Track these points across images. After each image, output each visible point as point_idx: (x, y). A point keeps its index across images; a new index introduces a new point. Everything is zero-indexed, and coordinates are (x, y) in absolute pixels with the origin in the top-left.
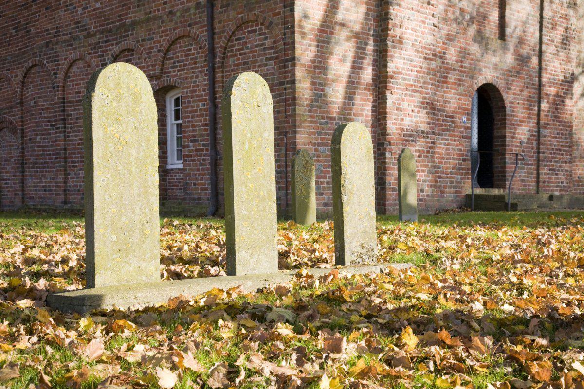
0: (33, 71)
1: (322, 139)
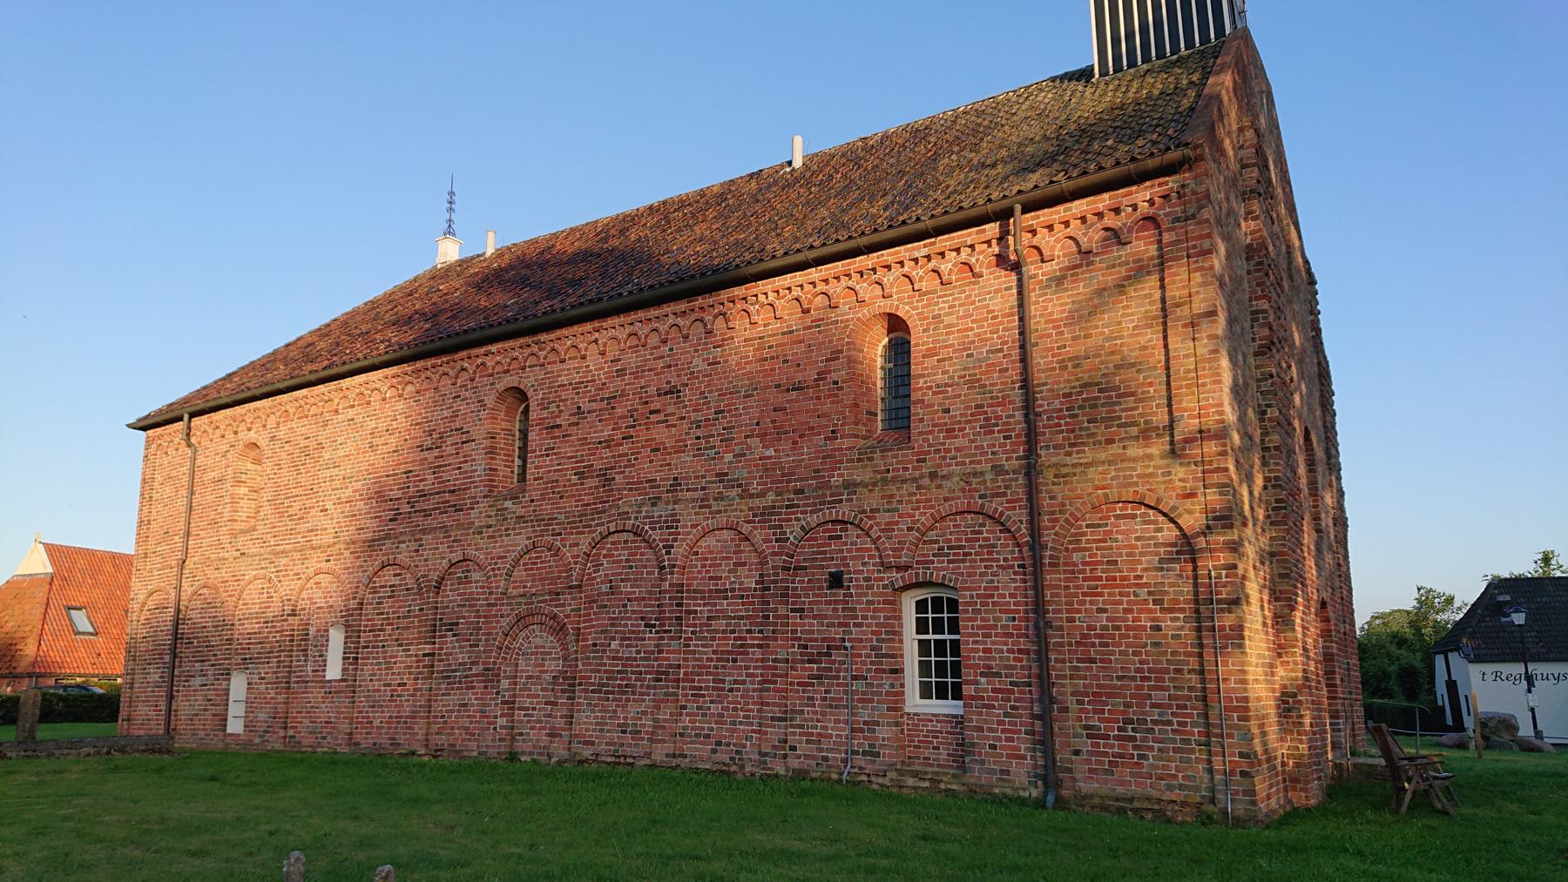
0: (610, 539)
1: (708, 442)
